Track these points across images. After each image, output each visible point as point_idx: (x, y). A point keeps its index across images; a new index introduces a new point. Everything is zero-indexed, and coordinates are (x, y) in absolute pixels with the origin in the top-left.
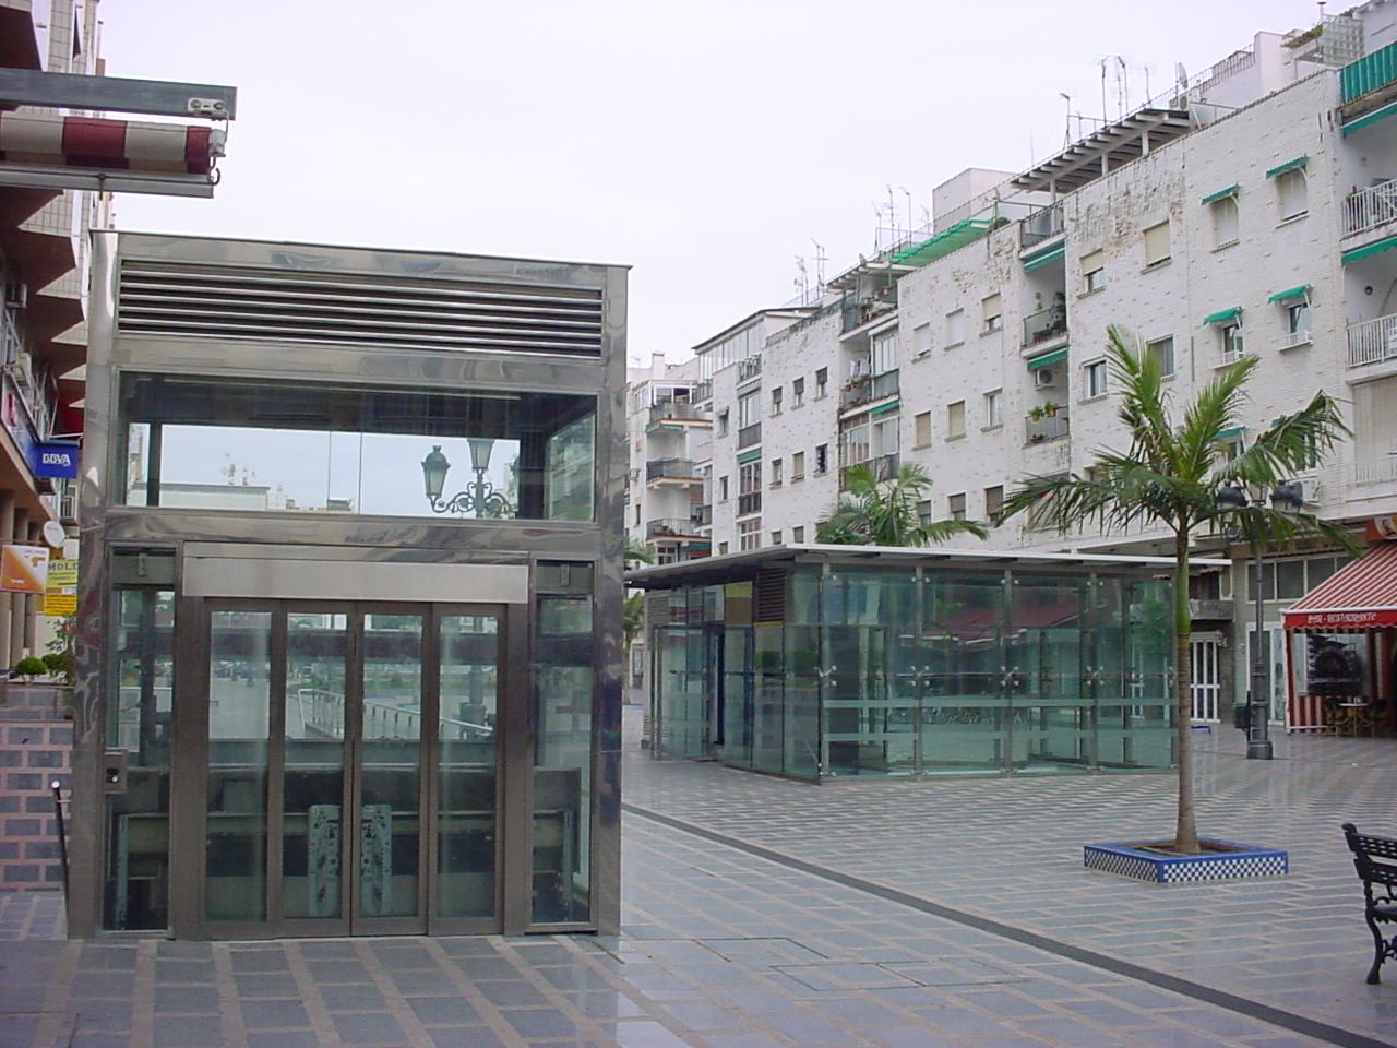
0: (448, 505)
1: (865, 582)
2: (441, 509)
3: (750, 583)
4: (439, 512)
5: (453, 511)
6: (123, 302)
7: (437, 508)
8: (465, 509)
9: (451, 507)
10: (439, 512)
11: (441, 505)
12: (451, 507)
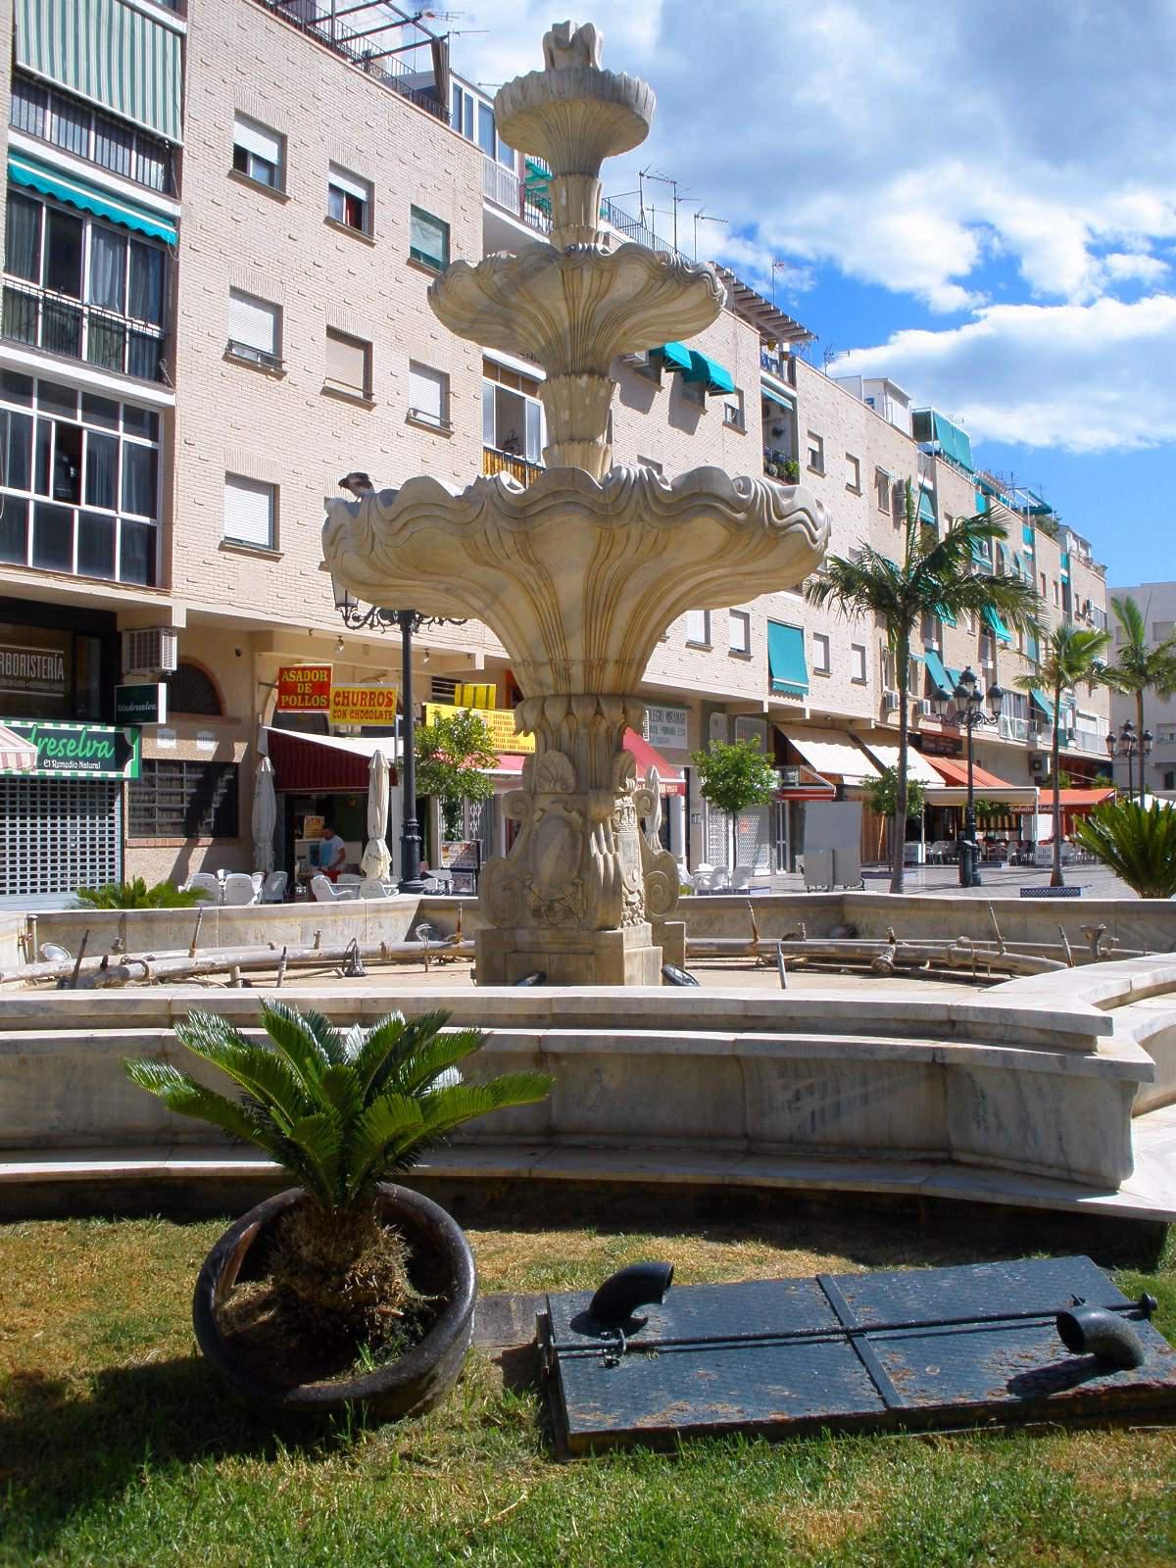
0: (366, 618)
1: (36, 773)
2: (357, 624)
3: (430, 281)
4: (354, 628)
5: (372, 626)
6: (434, 684)
7: (351, 623)
8: (387, 622)
9: (369, 622)
10: (354, 628)
11: (356, 619)
12: (369, 622)
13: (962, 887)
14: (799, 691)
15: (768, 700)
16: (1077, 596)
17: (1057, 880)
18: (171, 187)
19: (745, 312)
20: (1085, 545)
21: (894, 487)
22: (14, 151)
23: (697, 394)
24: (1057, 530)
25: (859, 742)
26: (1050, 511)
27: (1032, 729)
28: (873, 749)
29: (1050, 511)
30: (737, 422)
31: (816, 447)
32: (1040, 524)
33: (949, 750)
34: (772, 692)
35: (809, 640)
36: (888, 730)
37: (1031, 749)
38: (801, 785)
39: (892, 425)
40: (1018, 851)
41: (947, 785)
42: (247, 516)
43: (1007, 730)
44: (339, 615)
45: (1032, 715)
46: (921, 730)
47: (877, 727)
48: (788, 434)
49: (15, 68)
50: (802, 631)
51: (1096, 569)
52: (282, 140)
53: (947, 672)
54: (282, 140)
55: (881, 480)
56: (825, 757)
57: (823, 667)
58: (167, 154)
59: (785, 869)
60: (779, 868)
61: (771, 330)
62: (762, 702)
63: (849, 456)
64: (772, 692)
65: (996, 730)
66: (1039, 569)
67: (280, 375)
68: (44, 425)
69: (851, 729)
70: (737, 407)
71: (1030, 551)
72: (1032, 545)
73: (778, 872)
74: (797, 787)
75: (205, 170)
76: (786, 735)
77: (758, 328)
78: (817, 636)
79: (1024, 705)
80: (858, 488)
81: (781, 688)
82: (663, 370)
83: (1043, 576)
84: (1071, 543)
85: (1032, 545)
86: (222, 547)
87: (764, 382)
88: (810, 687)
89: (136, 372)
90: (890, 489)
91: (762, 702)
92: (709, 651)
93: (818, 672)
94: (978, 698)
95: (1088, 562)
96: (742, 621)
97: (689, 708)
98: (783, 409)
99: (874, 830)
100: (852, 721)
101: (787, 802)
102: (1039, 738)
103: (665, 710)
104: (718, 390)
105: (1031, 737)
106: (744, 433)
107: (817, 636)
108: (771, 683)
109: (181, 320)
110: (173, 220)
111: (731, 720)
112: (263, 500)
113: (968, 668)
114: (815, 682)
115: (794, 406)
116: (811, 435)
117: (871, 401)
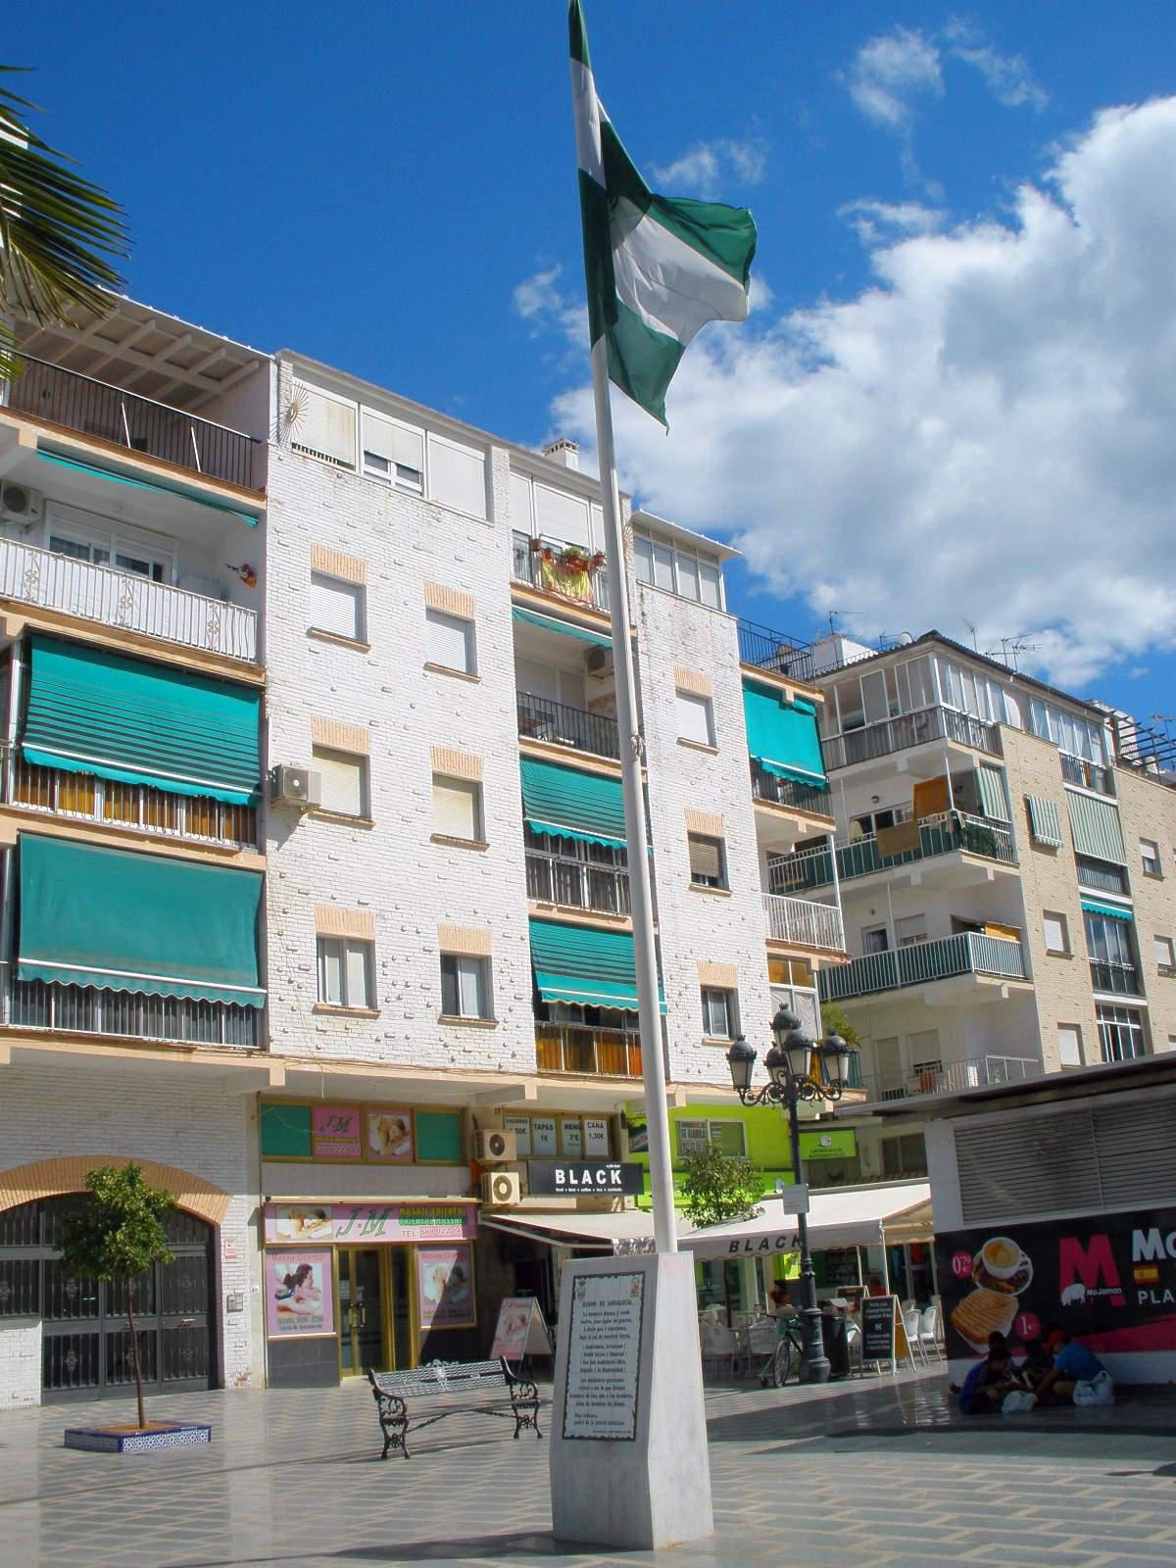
18: (1125, 890)
22: (1083, 895)
31: (1150, 853)
49: (1076, 853)
54: (1154, 845)
58: (1120, 872)
67: (954, 919)
68: (1106, 1025)
70: (1153, 857)
75: (1135, 878)
86: (710, 994)
89: (1120, 989)
96: (1074, 1032)
109: (1142, 960)
110: (1130, 907)
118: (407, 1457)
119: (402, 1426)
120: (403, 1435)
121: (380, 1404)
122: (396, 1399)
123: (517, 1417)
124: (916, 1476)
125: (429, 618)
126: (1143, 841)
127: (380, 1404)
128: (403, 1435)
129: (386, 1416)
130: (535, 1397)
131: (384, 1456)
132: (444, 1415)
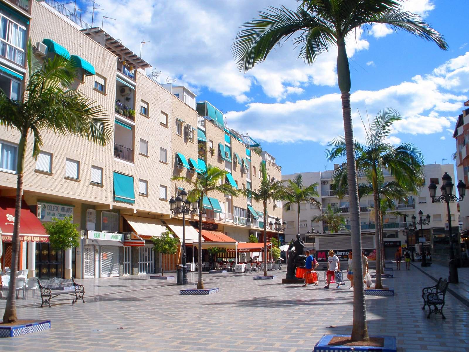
13: (178, 285)
14: (131, 202)
15: (112, 205)
16: (269, 176)
17: (265, 274)
19: (114, 49)
20: (273, 159)
21: (185, 127)
23: (80, 76)
24: (261, 152)
25: (166, 224)
26: (259, 146)
27: (248, 221)
28: (172, 227)
29: (259, 146)
30: (102, 89)
32: (255, 150)
33: (211, 228)
34: (114, 201)
35: (137, 182)
36: (178, 219)
37: (248, 228)
38: (132, 240)
39: (185, 104)
40: (231, 266)
41: (205, 241)
42: (96, 176)
43: (237, 221)
44: (171, 211)
45: (249, 216)
46: (195, 220)
47: (172, 218)
48: (132, 100)
50: (133, 177)
51: (277, 167)
52: (105, 79)
53: (209, 199)
54: (105, 79)
55: (179, 123)
56: (141, 229)
57: (145, 193)
59: (129, 273)
60: (126, 273)
61: (132, 62)
62: (133, 209)
63: (162, 112)
64: (114, 201)
65: (232, 221)
66: (252, 165)
69: (161, 218)
70: (103, 84)
71: (249, 158)
72: (250, 156)
73: (124, 275)
74: (130, 241)
76: (127, 220)
77: (117, 55)
78: (141, 180)
79: (245, 213)
80: (167, 125)
81: (119, 199)
82: (85, 75)
83: (254, 167)
84: (267, 157)
85: (250, 156)
87: (118, 76)
88: (136, 200)
90: (183, 128)
91: (133, 209)
92: (79, 182)
93: (141, 194)
94: (280, 224)
95: (274, 164)
97: (74, 206)
98: (130, 89)
99: (175, 258)
100: (162, 215)
101: (130, 247)
102: (252, 224)
103: (60, 206)
104: (89, 74)
105: (248, 224)
106: (105, 95)
107: (141, 180)
108: (114, 197)
111: (98, 213)
112: (100, 171)
113: (184, 189)
114: (138, 199)
115: (135, 89)
116: (142, 101)
117: (178, 95)
118: (50, 307)
119: (82, 294)
120: (49, 300)
121: (41, 290)
122: (81, 286)
123: (77, 296)
124: (105, 340)
125: (160, 124)
126: (142, 101)
127: (41, 290)
128: (49, 300)
129: (43, 294)
130: (83, 290)
131: (42, 307)
132: (59, 295)
